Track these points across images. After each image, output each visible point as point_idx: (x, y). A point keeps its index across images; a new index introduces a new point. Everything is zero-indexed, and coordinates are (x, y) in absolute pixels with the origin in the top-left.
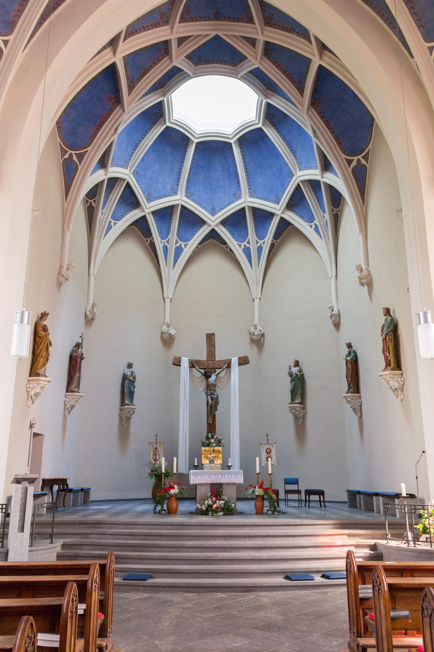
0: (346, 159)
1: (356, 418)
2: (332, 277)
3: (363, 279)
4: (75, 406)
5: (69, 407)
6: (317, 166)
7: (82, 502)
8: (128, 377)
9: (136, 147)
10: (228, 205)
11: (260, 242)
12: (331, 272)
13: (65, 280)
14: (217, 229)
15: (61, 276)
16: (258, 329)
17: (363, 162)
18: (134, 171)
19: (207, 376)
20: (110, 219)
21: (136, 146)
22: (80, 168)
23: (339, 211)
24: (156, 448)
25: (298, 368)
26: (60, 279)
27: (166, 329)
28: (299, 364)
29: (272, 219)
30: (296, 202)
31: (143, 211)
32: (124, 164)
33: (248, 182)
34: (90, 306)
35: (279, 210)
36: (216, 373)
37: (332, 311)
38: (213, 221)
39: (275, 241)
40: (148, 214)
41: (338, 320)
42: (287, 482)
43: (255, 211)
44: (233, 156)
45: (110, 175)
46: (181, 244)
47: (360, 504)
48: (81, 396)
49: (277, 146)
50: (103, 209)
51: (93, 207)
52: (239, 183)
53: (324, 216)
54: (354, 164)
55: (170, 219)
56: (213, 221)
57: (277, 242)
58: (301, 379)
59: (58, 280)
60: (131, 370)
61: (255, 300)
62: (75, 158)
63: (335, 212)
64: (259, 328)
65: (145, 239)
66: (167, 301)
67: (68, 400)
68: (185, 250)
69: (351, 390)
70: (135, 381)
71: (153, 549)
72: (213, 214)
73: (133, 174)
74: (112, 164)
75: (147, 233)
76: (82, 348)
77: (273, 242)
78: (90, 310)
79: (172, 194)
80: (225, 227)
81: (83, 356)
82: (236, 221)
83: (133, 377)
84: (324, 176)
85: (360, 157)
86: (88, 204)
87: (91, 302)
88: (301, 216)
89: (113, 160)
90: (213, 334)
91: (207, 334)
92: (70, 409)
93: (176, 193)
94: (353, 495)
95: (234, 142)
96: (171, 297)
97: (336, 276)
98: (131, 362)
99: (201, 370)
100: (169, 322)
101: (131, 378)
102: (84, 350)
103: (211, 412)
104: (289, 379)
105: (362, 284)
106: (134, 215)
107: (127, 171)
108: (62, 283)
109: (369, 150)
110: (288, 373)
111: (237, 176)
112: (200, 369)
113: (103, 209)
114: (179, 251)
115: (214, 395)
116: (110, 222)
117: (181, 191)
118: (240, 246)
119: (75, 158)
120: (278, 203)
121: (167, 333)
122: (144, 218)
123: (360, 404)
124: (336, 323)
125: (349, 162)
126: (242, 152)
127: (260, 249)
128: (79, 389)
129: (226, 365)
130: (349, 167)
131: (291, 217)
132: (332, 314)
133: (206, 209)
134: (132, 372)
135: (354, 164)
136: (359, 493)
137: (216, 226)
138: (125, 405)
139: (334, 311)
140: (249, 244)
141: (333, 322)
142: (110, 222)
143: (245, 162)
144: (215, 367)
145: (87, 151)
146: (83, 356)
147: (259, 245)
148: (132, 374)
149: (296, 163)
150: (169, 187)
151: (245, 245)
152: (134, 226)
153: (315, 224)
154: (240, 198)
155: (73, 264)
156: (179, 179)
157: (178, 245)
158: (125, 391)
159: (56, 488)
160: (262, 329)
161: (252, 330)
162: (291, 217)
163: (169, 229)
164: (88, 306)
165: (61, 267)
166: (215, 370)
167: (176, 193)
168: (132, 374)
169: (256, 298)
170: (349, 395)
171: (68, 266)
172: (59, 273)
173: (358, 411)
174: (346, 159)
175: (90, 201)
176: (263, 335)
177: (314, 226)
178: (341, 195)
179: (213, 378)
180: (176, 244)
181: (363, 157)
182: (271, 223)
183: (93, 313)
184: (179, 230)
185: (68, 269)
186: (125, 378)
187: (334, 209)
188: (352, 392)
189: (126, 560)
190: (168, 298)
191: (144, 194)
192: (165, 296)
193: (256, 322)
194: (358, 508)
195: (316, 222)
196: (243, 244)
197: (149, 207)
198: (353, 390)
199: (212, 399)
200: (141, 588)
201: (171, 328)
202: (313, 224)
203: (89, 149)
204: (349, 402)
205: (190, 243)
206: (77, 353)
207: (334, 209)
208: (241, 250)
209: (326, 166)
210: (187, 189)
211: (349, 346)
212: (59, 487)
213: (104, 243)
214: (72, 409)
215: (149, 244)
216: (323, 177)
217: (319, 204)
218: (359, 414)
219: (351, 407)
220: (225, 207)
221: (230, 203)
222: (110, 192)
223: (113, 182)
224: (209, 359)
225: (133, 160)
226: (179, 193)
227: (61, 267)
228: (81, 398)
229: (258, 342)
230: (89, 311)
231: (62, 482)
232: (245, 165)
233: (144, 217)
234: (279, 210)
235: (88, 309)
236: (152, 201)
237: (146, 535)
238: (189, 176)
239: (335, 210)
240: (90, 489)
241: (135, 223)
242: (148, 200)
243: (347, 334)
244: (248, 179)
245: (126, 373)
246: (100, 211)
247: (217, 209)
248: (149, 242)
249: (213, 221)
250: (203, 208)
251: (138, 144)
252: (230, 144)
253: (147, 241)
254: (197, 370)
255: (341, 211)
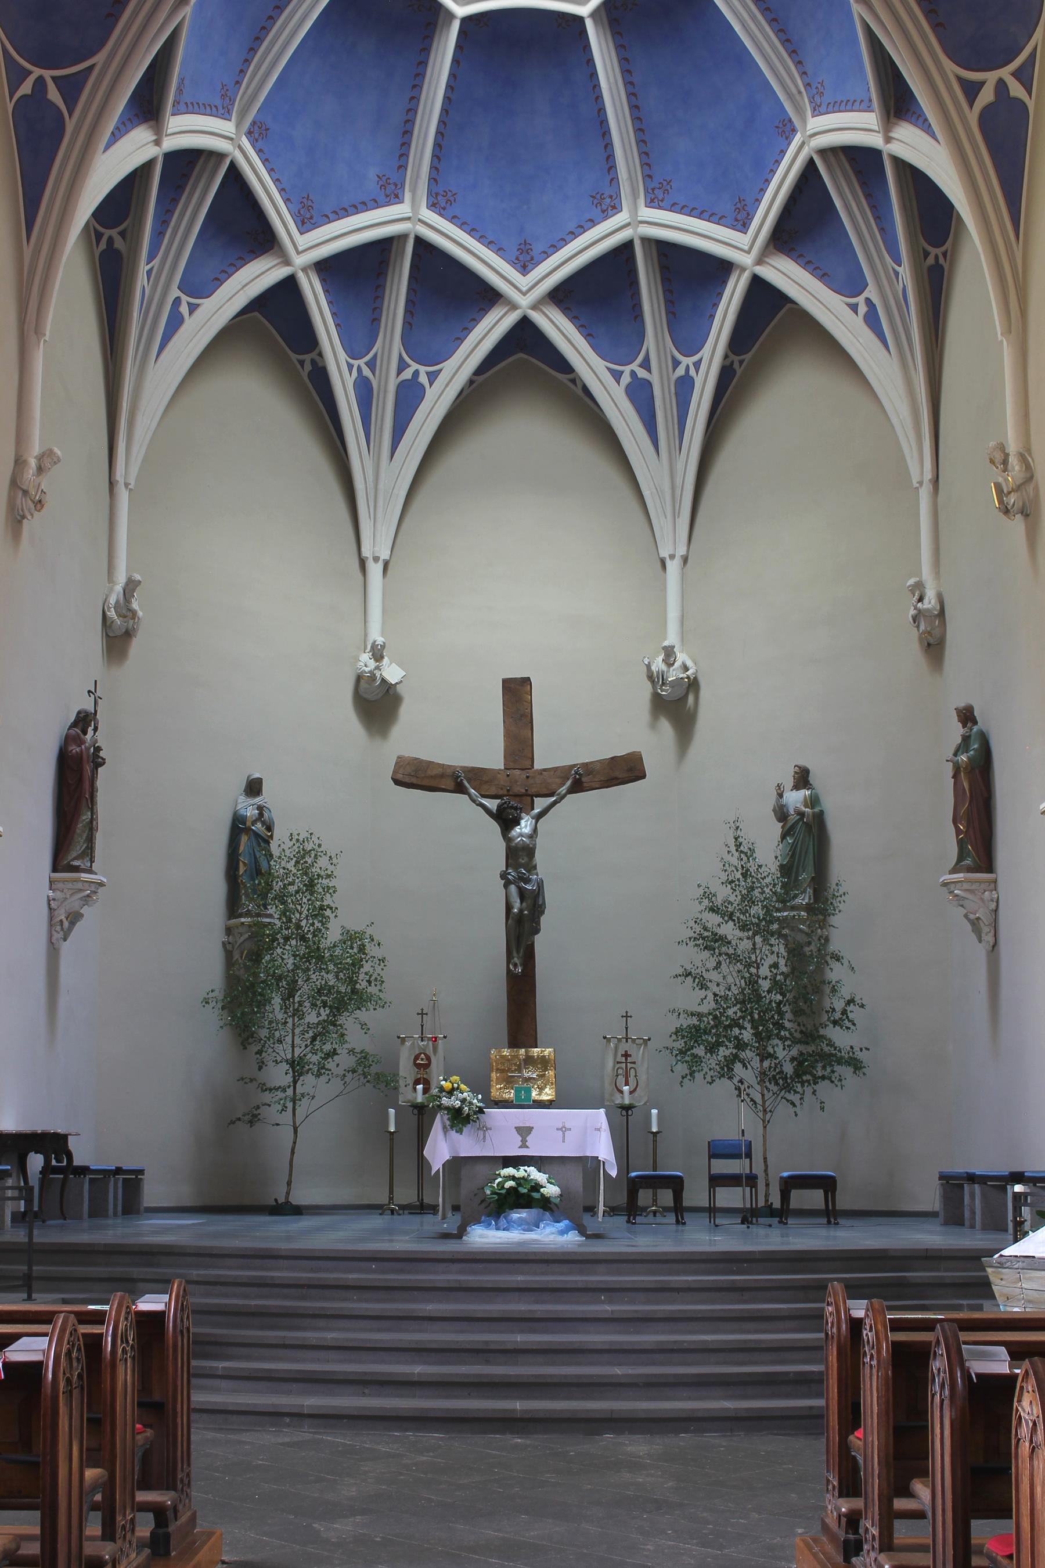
0: (960, 80)
1: (980, 952)
2: (921, 483)
3: (1009, 493)
4: (82, 915)
5: (63, 917)
6: (870, 100)
7: (120, 1208)
8: (248, 824)
9: (259, 39)
10: (574, 235)
11: (686, 361)
12: (920, 469)
13: (32, 506)
14: (537, 317)
15: (20, 494)
16: (677, 664)
17: (1016, 90)
18: (254, 123)
19: (506, 820)
20: (175, 293)
21: (257, 38)
22: (70, 126)
23: (945, 254)
24: (626, 1055)
25: (808, 793)
26: (19, 502)
27: (372, 664)
28: (811, 779)
29: (725, 282)
30: (803, 225)
31: (287, 262)
32: (218, 102)
33: (644, 154)
34: (119, 588)
35: (748, 252)
36: (536, 811)
37: (921, 599)
38: (524, 289)
39: (736, 359)
40: (304, 270)
41: (937, 632)
42: (717, 1151)
43: (671, 257)
44: (591, 61)
45: (170, 144)
46: (416, 373)
47: (973, 1213)
48: (101, 884)
49: (737, 28)
50: (151, 258)
51: (117, 254)
52: (610, 157)
53: (897, 274)
54: (986, 96)
55: (378, 287)
56: (524, 289)
57: (741, 362)
58: (815, 830)
59: (11, 506)
60: (257, 800)
61: (668, 563)
62: (54, 95)
63: (931, 260)
64: (681, 657)
65: (294, 357)
66: (375, 570)
67: (59, 895)
68: (431, 393)
69: (968, 862)
70: (271, 837)
71: (322, 1323)
72: (524, 267)
73: (249, 133)
74: (176, 103)
75: (301, 335)
76: (96, 729)
77: (728, 362)
78: (117, 602)
79: (381, 198)
80: (566, 310)
81: (102, 754)
82: (600, 293)
83: (263, 823)
84: (892, 135)
85: (1005, 73)
86: (103, 245)
87: (121, 579)
88: (821, 273)
89: (180, 90)
90: (527, 681)
91: (505, 681)
92: (66, 924)
93: (397, 196)
94: (954, 1185)
95: (594, 15)
96: (385, 555)
97: (936, 481)
98: (257, 775)
99: (484, 801)
100: (380, 640)
101: (258, 827)
102: (102, 737)
103: (519, 939)
104: (777, 828)
105: (1006, 511)
106: (257, 276)
107: (228, 127)
108: (24, 517)
109: (1035, 49)
110: (774, 810)
111: (606, 133)
112: (484, 796)
113: (151, 258)
114: (409, 397)
115: (527, 881)
116: (177, 301)
117: (414, 191)
118: (617, 376)
119: (54, 95)
120: (743, 226)
121: (373, 677)
122: (288, 289)
123: (993, 906)
124: (932, 641)
125: (971, 90)
126: (620, 47)
127: (685, 385)
128: (92, 862)
129: (569, 783)
130: (971, 106)
131: (787, 275)
132: (920, 611)
133: (499, 251)
134: (260, 808)
135: (986, 96)
136: (971, 1178)
137: (535, 307)
138: (240, 916)
139: (926, 601)
140: (649, 370)
141: (921, 639)
142: (177, 301)
143: (631, 83)
144: (533, 791)
145: (91, 68)
146: (102, 754)
147: (680, 371)
148: (261, 815)
149: (802, 89)
150: (372, 173)
151: (633, 373)
152: (256, 314)
153: (868, 301)
154: (616, 208)
155: (59, 453)
156: (406, 145)
157: (407, 374)
158: (242, 869)
159: (36, 1161)
160: (689, 663)
161: (658, 664)
162: (787, 275)
163: (376, 321)
164: (111, 590)
165: (19, 462)
166: (533, 802)
167: (396, 198)
168: (261, 815)
169: (672, 557)
170: (960, 876)
171: (40, 458)
172: (14, 483)
173: (985, 929)
174: (960, 80)
175: (107, 233)
176: (693, 685)
177: (863, 309)
178: (952, 206)
179: (525, 826)
180: (399, 374)
181: (1015, 74)
182: (720, 295)
183: (126, 611)
184: (408, 324)
185: (40, 470)
186: (238, 826)
187: (929, 248)
188: (969, 870)
189: (245, 1351)
190: (376, 559)
191: (287, 201)
192: (366, 552)
193: (672, 638)
194: (967, 1223)
195: (871, 292)
196: (627, 369)
197: (307, 246)
198: (974, 861)
199: (522, 894)
200: (288, 1420)
201: (386, 660)
202: (860, 300)
203: (99, 58)
204: (959, 900)
205: (449, 366)
206: (80, 746)
207: (929, 248)
208: (619, 392)
209: (898, 104)
210: (433, 180)
211: (967, 716)
212: (47, 1161)
213: (160, 376)
214: (73, 924)
215: (310, 375)
216: (888, 140)
217: (882, 230)
218: (990, 938)
219: (966, 916)
220: (565, 242)
221: (582, 229)
222: (175, 201)
223: (184, 165)
224: (512, 765)
225: (247, 88)
226: (407, 196)
227: (19, 462)
228: (101, 890)
229: (676, 705)
230: (117, 606)
231: (54, 1144)
232: (631, 95)
233: (290, 284)
234: (748, 252)
235: (112, 601)
236: (316, 226)
237: (302, 1286)
238: (439, 133)
239: (933, 251)
240: (141, 1172)
241: (261, 303)
242: (303, 223)
243: (961, 684)
244: (641, 142)
245: (242, 812)
246: (143, 268)
247: (537, 248)
248: (308, 367)
249: (524, 289)
250: (489, 244)
251: (265, 30)
252: (579, 20)
253: (302, 363)
254: (474, 801)
255: (951, 256)
